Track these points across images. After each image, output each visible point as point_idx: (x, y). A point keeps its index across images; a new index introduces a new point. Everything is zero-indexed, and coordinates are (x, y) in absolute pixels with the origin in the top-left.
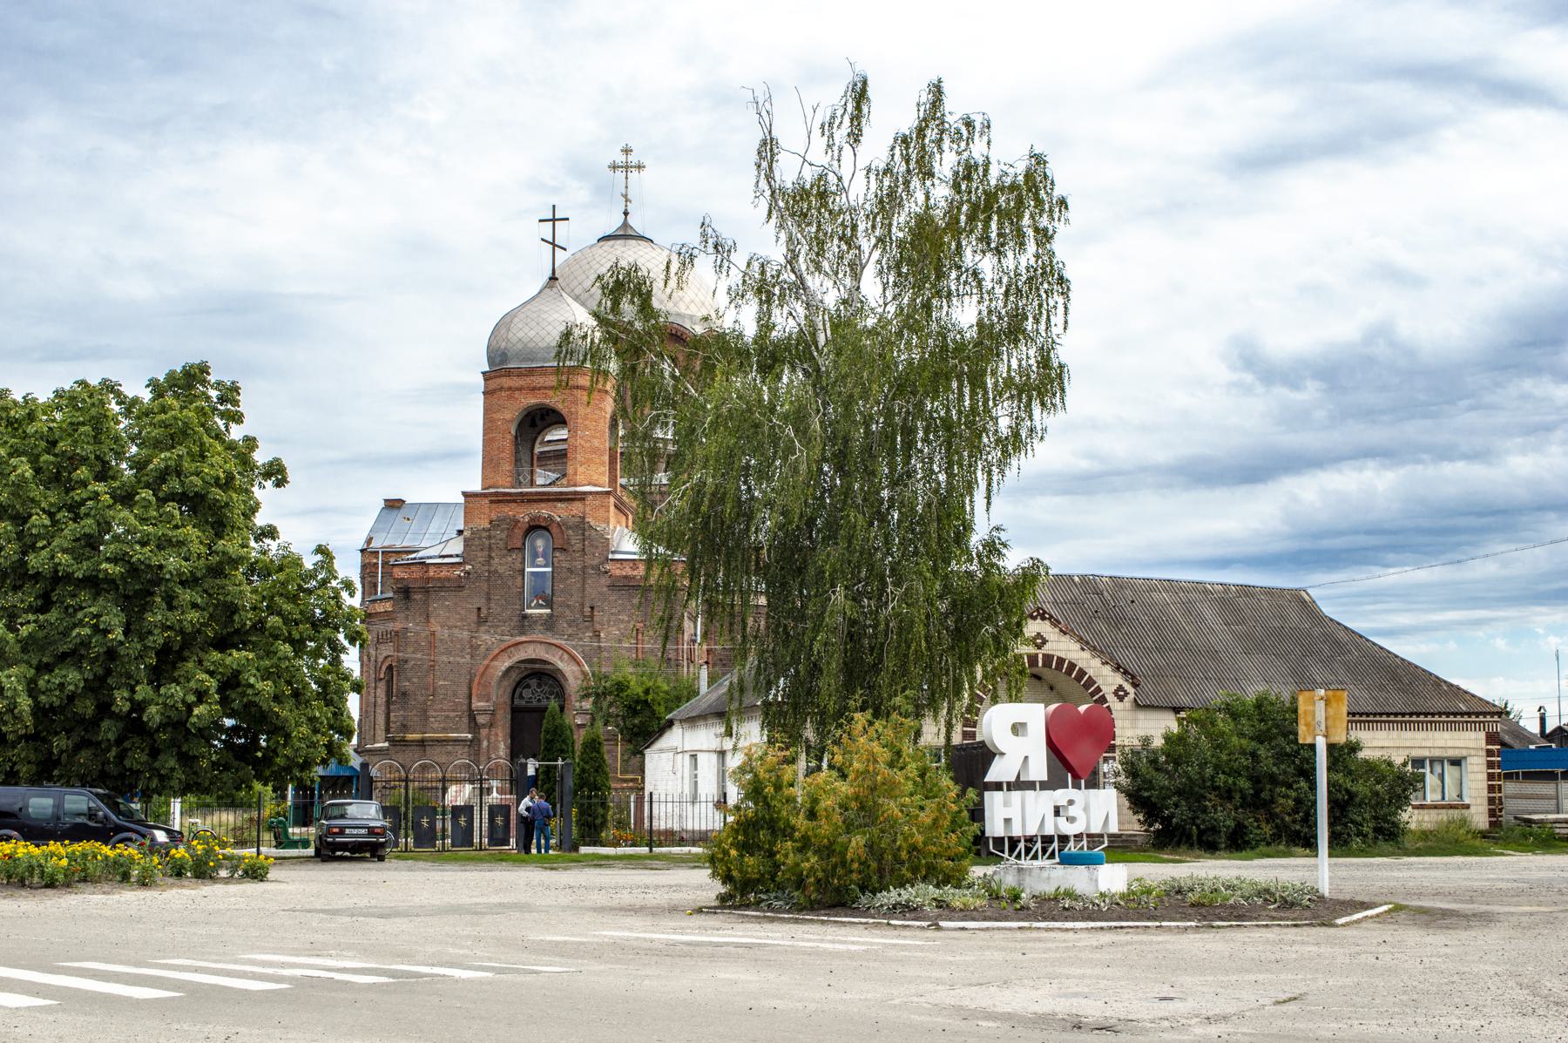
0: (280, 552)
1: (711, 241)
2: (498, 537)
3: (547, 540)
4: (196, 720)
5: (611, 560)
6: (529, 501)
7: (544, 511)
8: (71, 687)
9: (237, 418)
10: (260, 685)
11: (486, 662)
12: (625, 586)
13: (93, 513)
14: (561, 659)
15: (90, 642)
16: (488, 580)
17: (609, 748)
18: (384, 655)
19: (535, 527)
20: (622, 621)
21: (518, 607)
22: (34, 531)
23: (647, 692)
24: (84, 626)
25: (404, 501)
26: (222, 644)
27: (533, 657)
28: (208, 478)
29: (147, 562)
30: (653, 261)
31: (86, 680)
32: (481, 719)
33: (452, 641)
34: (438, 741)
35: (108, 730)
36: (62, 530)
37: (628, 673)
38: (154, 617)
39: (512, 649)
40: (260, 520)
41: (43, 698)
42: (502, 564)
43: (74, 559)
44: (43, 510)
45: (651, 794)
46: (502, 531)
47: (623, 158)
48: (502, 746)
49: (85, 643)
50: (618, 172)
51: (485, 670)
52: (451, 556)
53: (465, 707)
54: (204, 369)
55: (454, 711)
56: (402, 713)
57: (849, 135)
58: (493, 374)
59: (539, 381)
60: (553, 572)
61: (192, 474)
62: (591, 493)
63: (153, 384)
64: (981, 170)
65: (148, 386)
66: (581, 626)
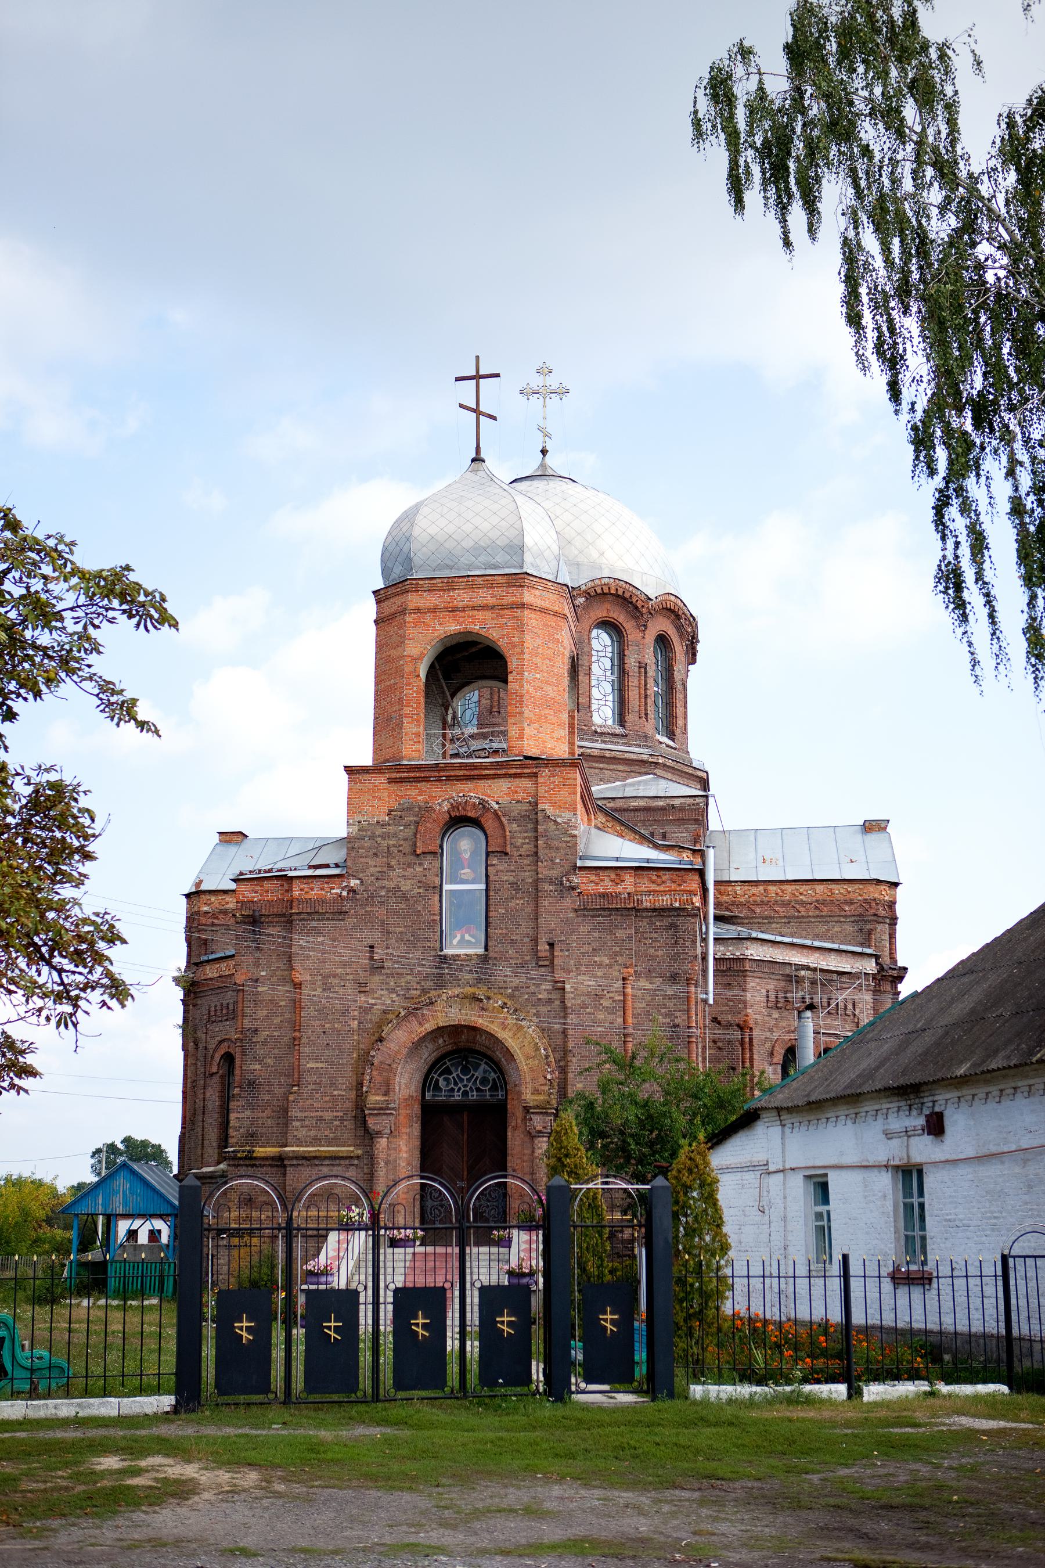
2: (401, 836)
5: (581, 868)
6: (449, 778)
7: (474, 792)
18: (219, 1039)
19: (458, 820)
20: (600, 965)
45: (845, 1258)
46: (406, 826)
52: (327, 866)
55: (331, 1109)
56: (248, 1113)
58: (390, 591)
59: (462, 597)
60: (487, 890)
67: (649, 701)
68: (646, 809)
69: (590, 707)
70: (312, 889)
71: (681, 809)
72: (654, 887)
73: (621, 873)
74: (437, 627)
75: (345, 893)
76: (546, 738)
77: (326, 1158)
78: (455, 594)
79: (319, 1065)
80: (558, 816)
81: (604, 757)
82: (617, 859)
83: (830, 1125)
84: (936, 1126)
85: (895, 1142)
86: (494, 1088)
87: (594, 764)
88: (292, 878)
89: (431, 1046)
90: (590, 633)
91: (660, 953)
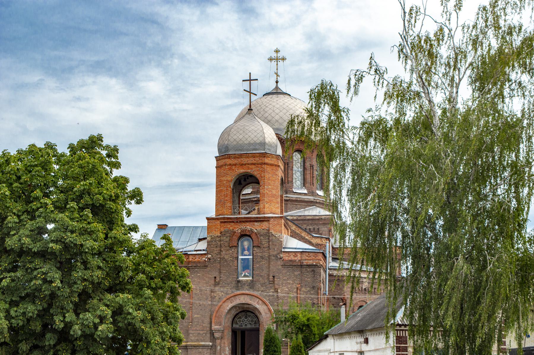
0: (143, 239)
1: (374, 68)
3: (250, 242)
4: (100, 333)
5: (283, 252)
6: (240, 222)
7: (248, 227)
8: (30, 314)
9: (117, 165)
10: (135, 313)
11: (220, 304)
12: (291, 265)
13: (43, 215)
14: (258, 303)
15: (41, 289)
16: (220, 263)
17: (284, 350)
19: (244, 235)
20: (289, 284)
21: (235, 276)
22: (10, 225)
23: (308, 320)
24: (37, 280)
25: (167, 226)
26: (111, 290)
27: (244, 302)
28: (106, 196)
29: (75, 242)
30: (292, 104)
31: (39, 311)
32: (217, 335)
33: (201, 294)
34: (195, 346)
35: (50, 340)
36: (25, 225)
37: (297, 310)
38: (78, 274)
39: (233, 298)
40: (128, 221)
41: (13, 321)
42: (227, 254)
43: (32, 241)
44: (14, 214)
46: (227, 237)
47: (275, 55)
48: (227, 349)
49: (38, 289)
50: (273, 62)
51: (219, 309)
52: (201, 250)
53: (208, 329)
54: (100, 138)
55: (202, 330)
57: (455, 6)
59: (245, 160)
60: (253, 258)
61: (96, 194)
62: (272, 217)
63: (72, 147)
64: (517, 30)
65: (68, 148)
66: (268, 286)
67: (314, 179)
68: (312, 220)
69: (292, 182)
70: (196, 258)
71: (325, 220)
72: (307, 258)
73: (297, 253)
74: (237, 170)
75: (206, 260)
76: (273, 207)
77: (201, 346)
78: (242, 159)
79: (198, 316)
80: (277, 234)
81: (297, 200)
82: (295, 249)
83: (345, 339)
84: (366, 341)
85: (359, 345)
86: (255, 323)
87: (294, 203)
88: (189, 254)
89: (235, 310)
90: (293, 154)
91: (309, 279)
